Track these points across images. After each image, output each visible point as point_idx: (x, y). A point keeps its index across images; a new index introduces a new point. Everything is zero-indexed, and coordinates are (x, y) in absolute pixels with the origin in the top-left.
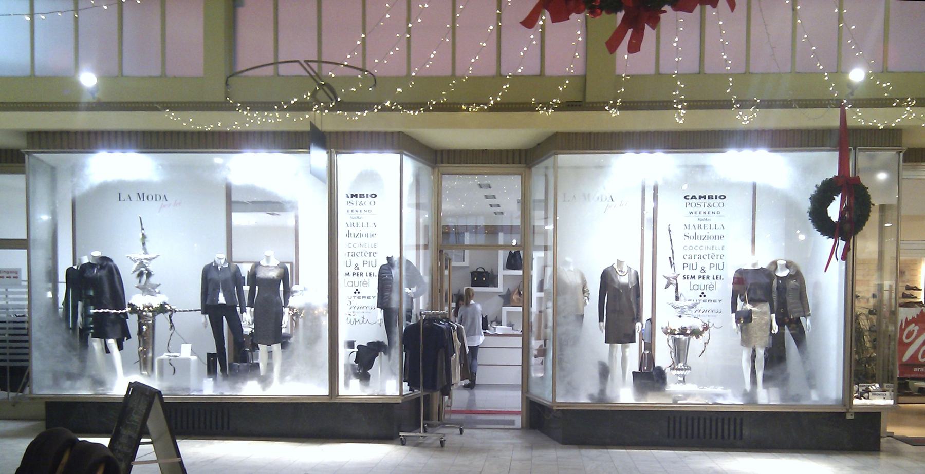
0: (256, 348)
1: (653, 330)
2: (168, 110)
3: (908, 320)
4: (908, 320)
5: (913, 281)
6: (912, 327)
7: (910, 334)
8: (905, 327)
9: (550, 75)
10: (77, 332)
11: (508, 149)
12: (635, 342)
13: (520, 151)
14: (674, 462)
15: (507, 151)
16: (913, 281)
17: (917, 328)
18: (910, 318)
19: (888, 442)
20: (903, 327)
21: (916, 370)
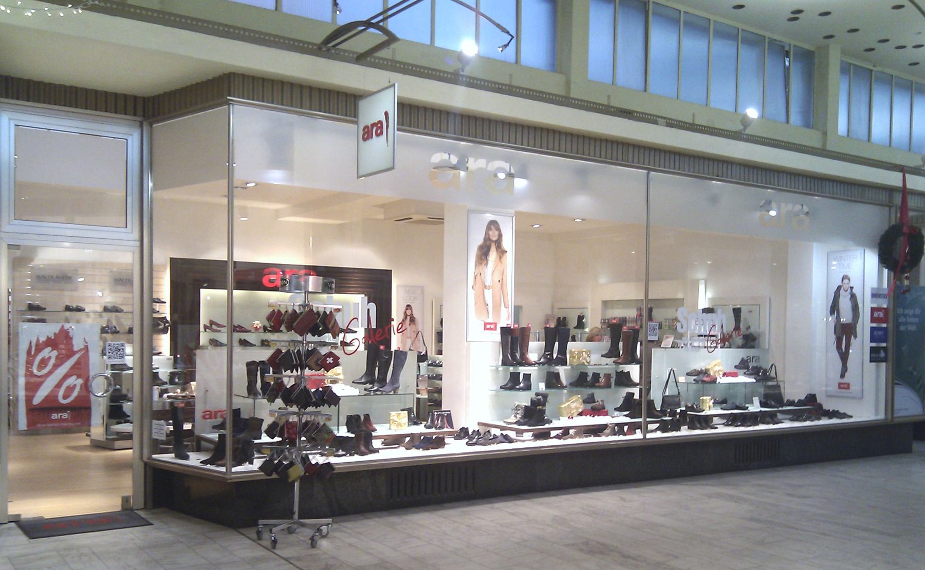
0: (112, 369)
1: (230, 337)
2: (70, 6)
3: (41, 342)
4: (41, 342)
5: (159, 285)
6: (46, 352)
7: (44, 363)
8: (35, 352)
9: (877, 285)
10: (435, 321)
11: (108, 90)
12: (501, 328)
13: (135, 98)
14: (133, 540)
15: (106, 94)
16: (159, 285)
17: (55, 353)
18: (43, 339)
19: (314, 458)
20: (33, 353)
21: (55, 416)
